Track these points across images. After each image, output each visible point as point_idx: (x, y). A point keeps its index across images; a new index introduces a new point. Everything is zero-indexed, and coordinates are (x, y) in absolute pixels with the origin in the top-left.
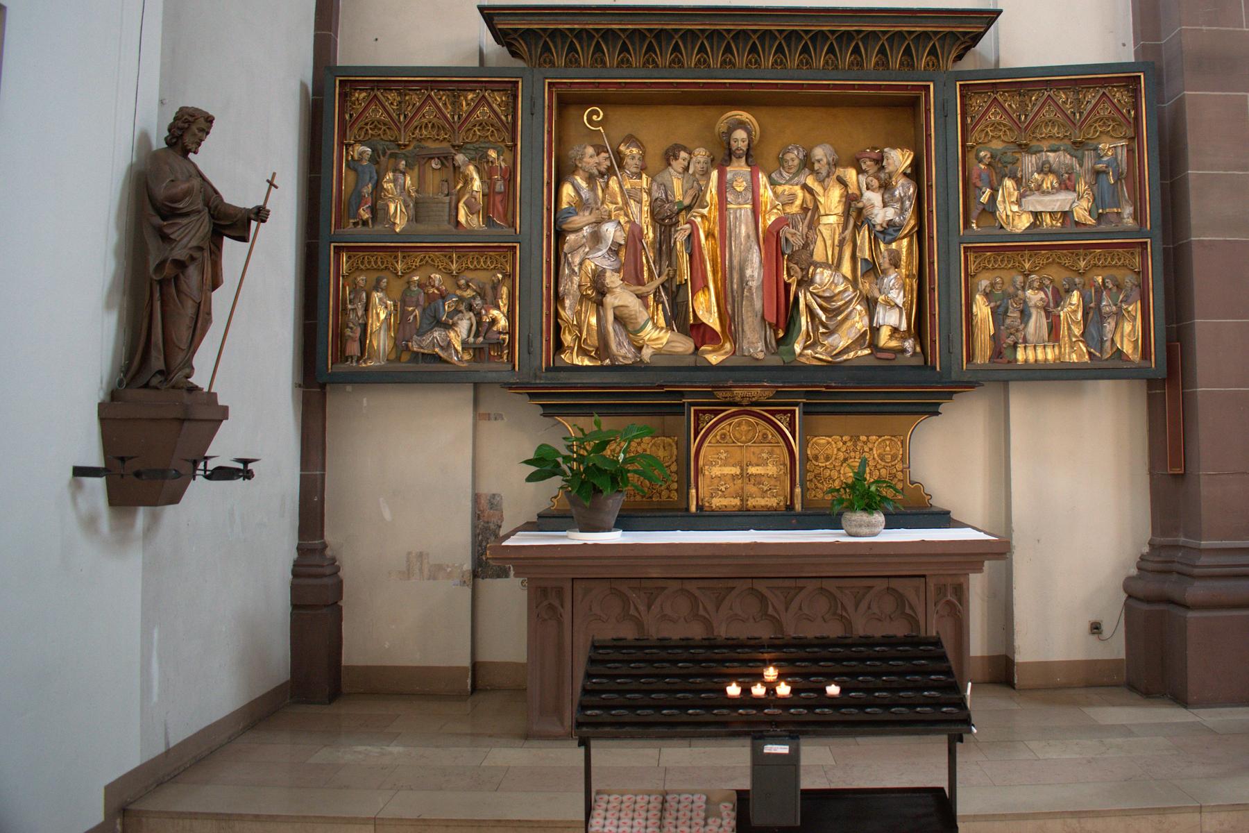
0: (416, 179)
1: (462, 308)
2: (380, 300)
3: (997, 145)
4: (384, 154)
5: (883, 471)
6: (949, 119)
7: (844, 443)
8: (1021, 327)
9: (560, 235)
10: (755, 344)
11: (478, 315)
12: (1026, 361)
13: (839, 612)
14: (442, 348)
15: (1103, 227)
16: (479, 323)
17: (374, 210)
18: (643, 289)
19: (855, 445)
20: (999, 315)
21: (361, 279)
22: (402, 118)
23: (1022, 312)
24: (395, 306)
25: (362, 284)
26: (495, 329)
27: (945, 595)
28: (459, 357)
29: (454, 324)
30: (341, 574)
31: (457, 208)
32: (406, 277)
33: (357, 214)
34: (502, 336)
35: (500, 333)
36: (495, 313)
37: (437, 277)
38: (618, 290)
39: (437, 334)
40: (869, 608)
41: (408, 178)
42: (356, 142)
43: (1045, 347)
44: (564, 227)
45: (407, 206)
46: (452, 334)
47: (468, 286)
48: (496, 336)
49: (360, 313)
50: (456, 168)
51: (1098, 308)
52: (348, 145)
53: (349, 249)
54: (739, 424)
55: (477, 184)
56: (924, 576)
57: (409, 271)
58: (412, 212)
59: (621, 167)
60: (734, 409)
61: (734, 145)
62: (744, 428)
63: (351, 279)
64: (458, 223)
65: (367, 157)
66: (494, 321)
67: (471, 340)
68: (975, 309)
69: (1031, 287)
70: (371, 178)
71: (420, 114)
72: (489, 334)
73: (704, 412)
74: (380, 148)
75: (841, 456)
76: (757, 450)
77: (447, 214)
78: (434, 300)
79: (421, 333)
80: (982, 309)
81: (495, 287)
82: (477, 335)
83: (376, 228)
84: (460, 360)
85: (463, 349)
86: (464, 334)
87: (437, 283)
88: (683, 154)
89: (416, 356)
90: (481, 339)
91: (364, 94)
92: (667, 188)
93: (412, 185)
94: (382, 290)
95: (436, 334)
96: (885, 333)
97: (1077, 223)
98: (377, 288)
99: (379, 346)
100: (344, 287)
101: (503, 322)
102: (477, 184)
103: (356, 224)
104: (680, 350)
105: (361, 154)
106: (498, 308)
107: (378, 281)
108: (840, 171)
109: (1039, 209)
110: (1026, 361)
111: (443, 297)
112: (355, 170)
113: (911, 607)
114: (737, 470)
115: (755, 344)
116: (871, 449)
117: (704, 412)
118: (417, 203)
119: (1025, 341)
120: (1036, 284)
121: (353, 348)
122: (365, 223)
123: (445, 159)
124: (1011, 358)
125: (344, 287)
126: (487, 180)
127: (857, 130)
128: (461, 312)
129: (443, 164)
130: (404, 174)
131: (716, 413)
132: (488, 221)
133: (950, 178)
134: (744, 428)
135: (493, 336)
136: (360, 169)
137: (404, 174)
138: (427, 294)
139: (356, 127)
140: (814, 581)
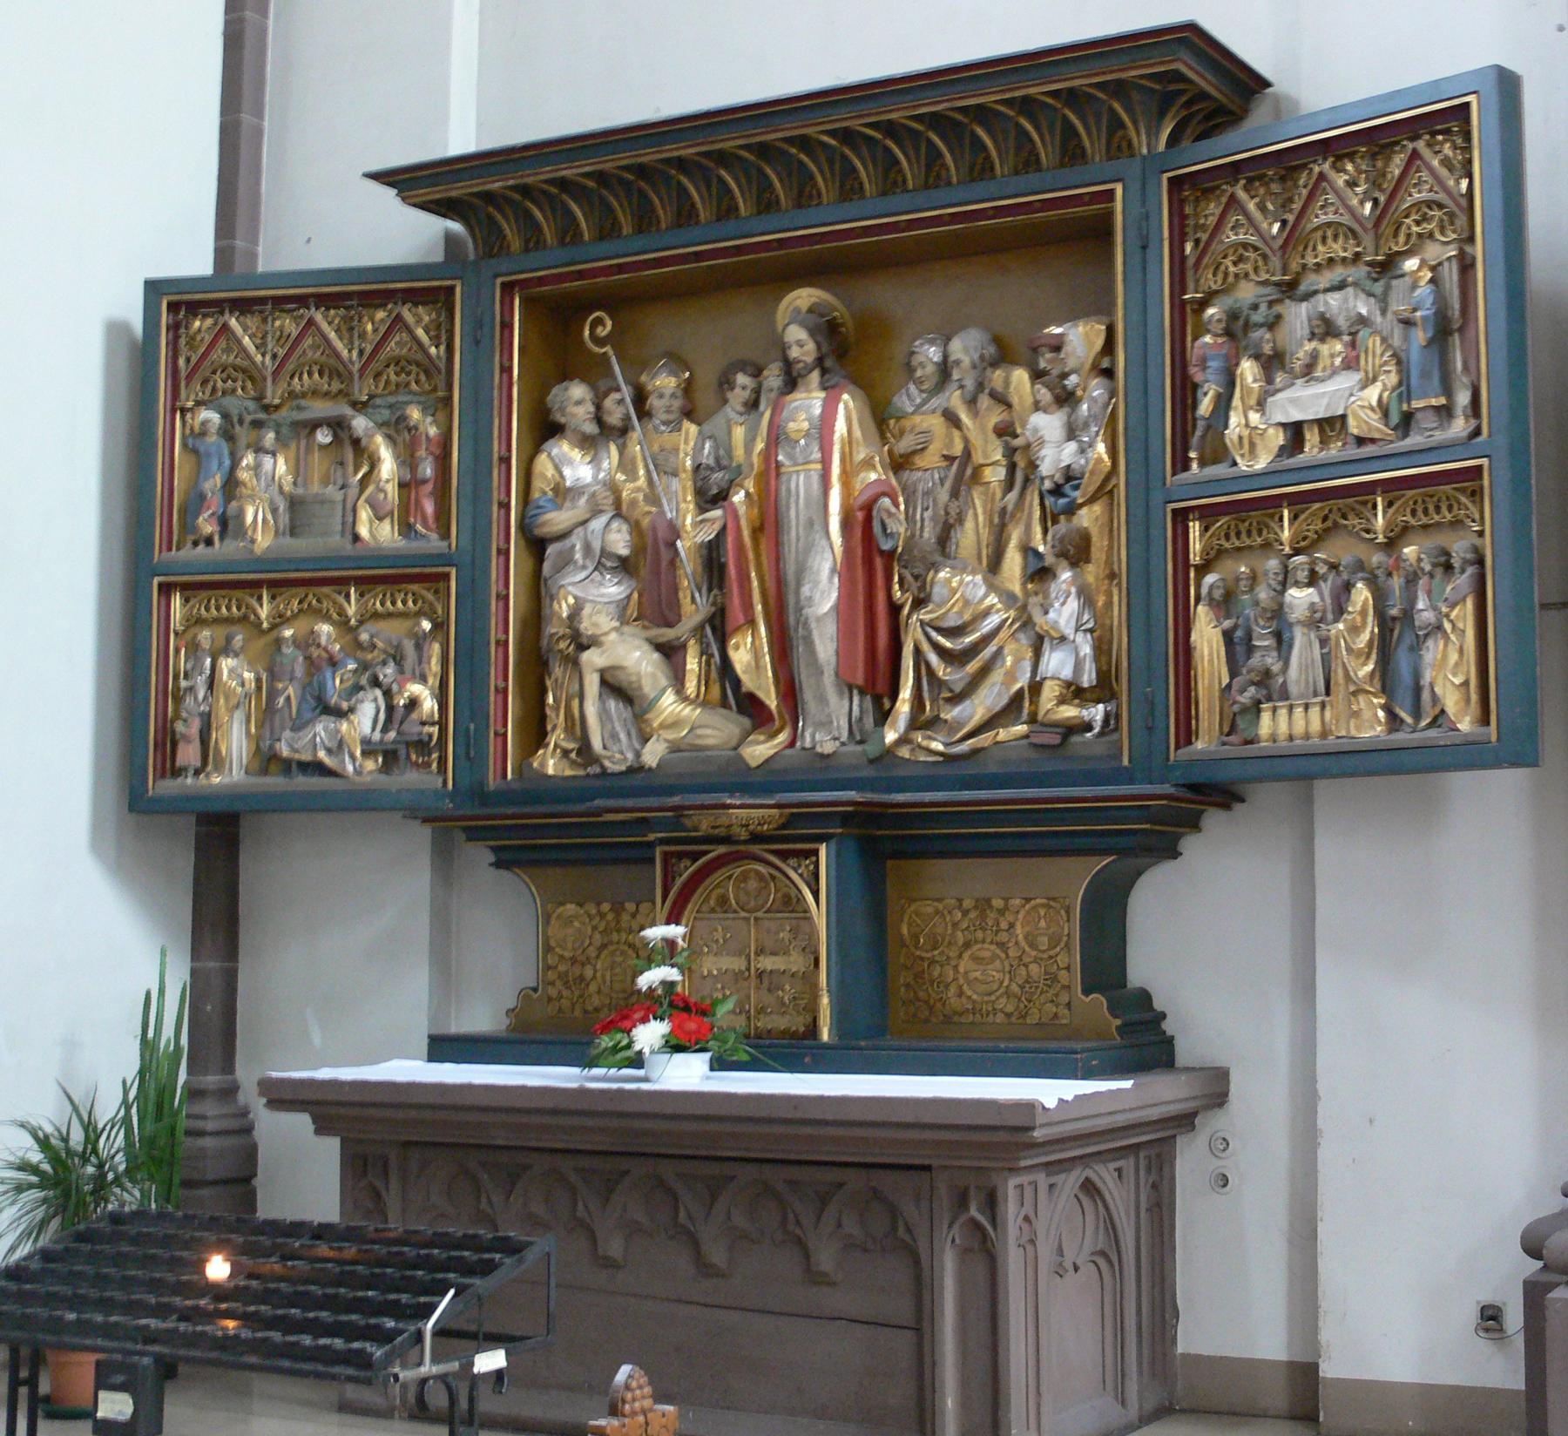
0: (292, 463)
1: (364, 681)
2: (231, 671)
3: (1246, 293)
4: (241, 422)
5: (1034, 968)
6: (1151, 253)
7: (965, 913)
8: (1276, 668)
9: (537, 546)
10: (831, 721)
11: (388, 694)
12: (1273, 738)
13: (791, 1227)
14: (329, 751)
15: (1415, 440)
16: (390, 708)
17: (224, 522)
18: (668, 634)
19: (983, 916)
20: (1237, 646)
21: (205, 635)
22: (355, 354)
23: (1278, 635)
24: (258, 680)
25: (206, 645)
26: (414, 716)
27: (967, 1209)
28: (360, 769)
29: (352, 710)
30: (256, 1133)
31: (354, 510)
32: (274, 634)
33: (195, 529)
34: (428, 729)
35: (423, 724)
36: (415, 689)
37: (325, 629)
38: (613, 636)
39: (321, 729)
40: (839, 1225)
41: (281, 461)
42: (199, 403)
43: (1307, 707)
44: (538, 532)
45: (274, 511)
46: (344, 726)
47: (374, 646)
48: (418, 729)
49: (201, 696)
50: (356, 442)
51: (1408, 614)
52: (183, 411)
53: (185, 588)
54: (744, 877)
55: (388, 466)
56: (928, 1168)
57: (280, 620)
58: (284, 519)
59: (643, 413)
60: (722, 849)
61: (794, 353)
62: (753, 884)
63: (189, 636)
64: (356, 538)
65: (213, 429)
66: (413, 703)
67: (377, 736)
68: (1193, 638)
69: (1297, 584)
70: (220, 464)
71: (299, 351)
72: (405, 727)
73: (681, 856)
74: (235, 413)
75: (960, 938)
76: (773, 925)
77: (338, 519)
78: (319, 664)
79: (299, 726)
80: (1207, 635)
81: (420, 642)
82: (385, 730)
83: (182, 553)
84: (358, 772)
85: (364, 753)
86: (366, 728)
87: (323, 640)
88: (742, 379)
89: (287, 766)
90: (392, 735)
91: (209, 321)
92: (723, 446)
93: (288, 471)
94: (236, 655)
95: (319, 728)
96: (1050, 692)
97: (1361, 441)
98: (226, 650)
99: (229, 749)
100: (177, 651)
101: (429, 705)
102: (388, 466)
103: (195, 544)
104: (711, 742)
105: (204, 423)
106: (423, 679)
107: (229, 639)
108: (997, 376)
109: (1296, 415)
110: (1273, 738)
111: (333, 663)
112: (195, 451)
113: (909, 1230)
114: (738, 964)
115: (831, 721)
116: (1012, 926)
117: (681, 856)
118: (294, 503)
119: (1284, 695)
120: (1302, 575)
121: (188, 754)
122: (209, 542)
123: (338, 426)
124: (1248, 735)
125: (177, 651)
126: (407, 459)
127: (1010, 291)
128: (362, 688)
129: (335, 436)
130: (274, 455)
131: (695, 857)
132: (406, 529)
133: (1152, 372)
134: (753, 884)
135: (412, 729)
136: (202, 449)
137: (274, 455)
138: (308, 658)
139: (198, 378)
140: (750, 1167)
